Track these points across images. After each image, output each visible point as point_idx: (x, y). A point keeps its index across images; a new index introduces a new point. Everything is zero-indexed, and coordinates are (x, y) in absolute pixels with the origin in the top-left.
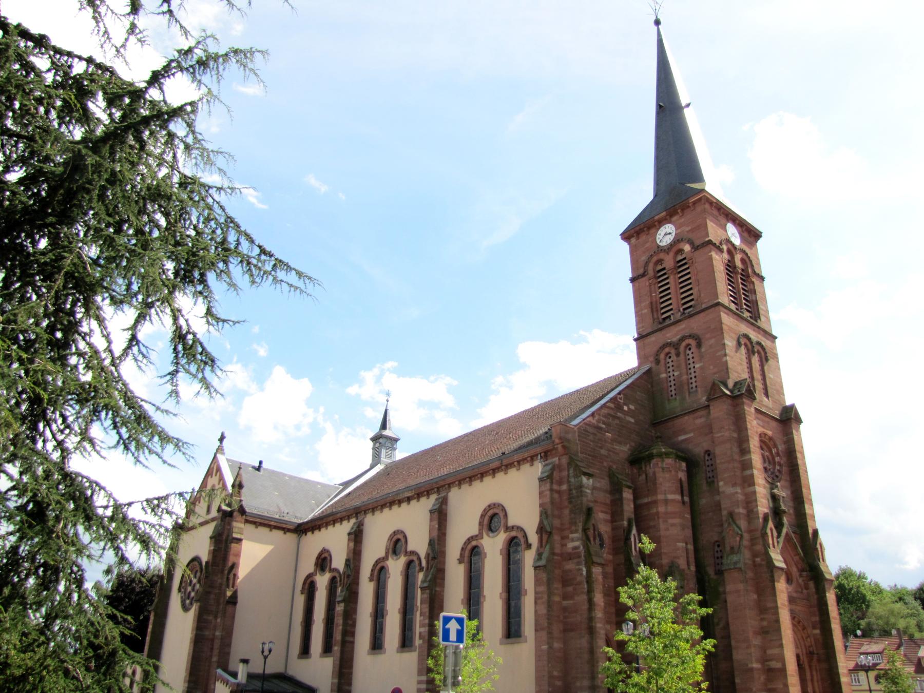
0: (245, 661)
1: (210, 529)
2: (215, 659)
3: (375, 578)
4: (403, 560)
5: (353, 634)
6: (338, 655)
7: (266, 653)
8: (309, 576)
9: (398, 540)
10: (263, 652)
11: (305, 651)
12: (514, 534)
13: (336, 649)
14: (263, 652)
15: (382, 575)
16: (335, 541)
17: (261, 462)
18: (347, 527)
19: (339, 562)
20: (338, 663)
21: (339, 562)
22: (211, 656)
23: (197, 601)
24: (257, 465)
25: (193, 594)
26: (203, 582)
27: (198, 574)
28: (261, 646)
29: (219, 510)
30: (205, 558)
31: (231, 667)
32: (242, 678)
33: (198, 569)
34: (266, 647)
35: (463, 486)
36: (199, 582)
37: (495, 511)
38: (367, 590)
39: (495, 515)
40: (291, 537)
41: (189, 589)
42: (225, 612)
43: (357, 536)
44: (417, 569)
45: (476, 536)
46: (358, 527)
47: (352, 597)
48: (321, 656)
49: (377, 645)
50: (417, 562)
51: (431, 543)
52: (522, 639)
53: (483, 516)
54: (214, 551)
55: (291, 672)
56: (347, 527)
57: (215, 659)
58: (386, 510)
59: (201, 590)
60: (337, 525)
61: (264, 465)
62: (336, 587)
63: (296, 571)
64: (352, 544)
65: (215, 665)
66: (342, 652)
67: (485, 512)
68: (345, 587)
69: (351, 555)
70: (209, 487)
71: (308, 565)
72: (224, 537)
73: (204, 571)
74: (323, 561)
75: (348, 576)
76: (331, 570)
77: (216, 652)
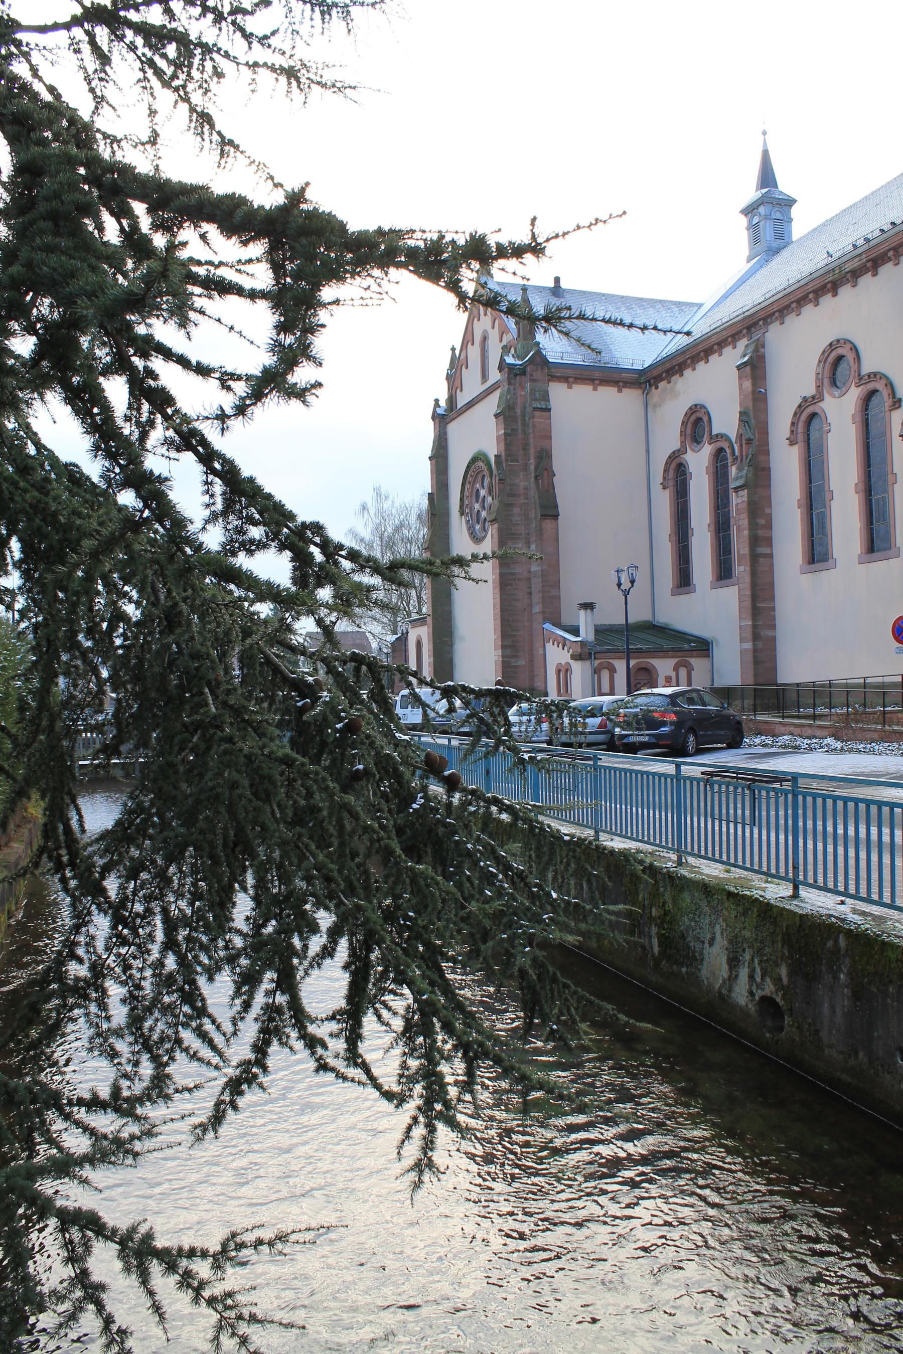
0: (588, 606)
1: (492, 404)
2: (537, 609)
3: (800, 437)
4: (707, 450)
6: (747, 579)
8: (806, 402)
9: (840, 358)
10: (619, 585)
11: (684, 580)
12: (719, 444)
13: (741, 570)
14: (619, 585)
16: (716, 387)
17: (557, 280)
18: (734, 355)
19: (726, 421)
20: (748, 592)
21: (726, 421)
23: (492, 521)
24: (552, 285)
25: (484, 514)
26: (496, 490)
27: (487, 481)
28: (614, 575)
30: (492, 449)
31: (566, 620)
33: (486, 473)
34: (624, 579)
36: (490, 492)
37: (840, 351)
38: (786, 464)
39: (840, 358)
40: (631, 397)
42: (540, 532)
43: (755, 369)
44: (888, 402)
46: (756, 350)
47: (760, 477)
48: (674, 594)
49: (817, 553)
50: (885, 393)
51: (744, 418)
52: (892, 552)
53: (684, 423)
54: (506, 434)
55: (663, 618)
56: (734, 355)
57: (537, 609)
58: (701, 366)
59: (496, 502)
60: (714, 358)
61: (563, 285)
62: (725, 467)
63: (648, 452)
64: (748, 384)
65: (540, 618)
66: (754, 573)
67: (825, 354)
68: (744, 464)
69: (750, 404)
70: (478, 338)
71: (668, 437)
72: (519, 411)
73: (495, 472)
74: (696, 424)
75: (749, 441)
76: (715, 438)
77: (537, 597)
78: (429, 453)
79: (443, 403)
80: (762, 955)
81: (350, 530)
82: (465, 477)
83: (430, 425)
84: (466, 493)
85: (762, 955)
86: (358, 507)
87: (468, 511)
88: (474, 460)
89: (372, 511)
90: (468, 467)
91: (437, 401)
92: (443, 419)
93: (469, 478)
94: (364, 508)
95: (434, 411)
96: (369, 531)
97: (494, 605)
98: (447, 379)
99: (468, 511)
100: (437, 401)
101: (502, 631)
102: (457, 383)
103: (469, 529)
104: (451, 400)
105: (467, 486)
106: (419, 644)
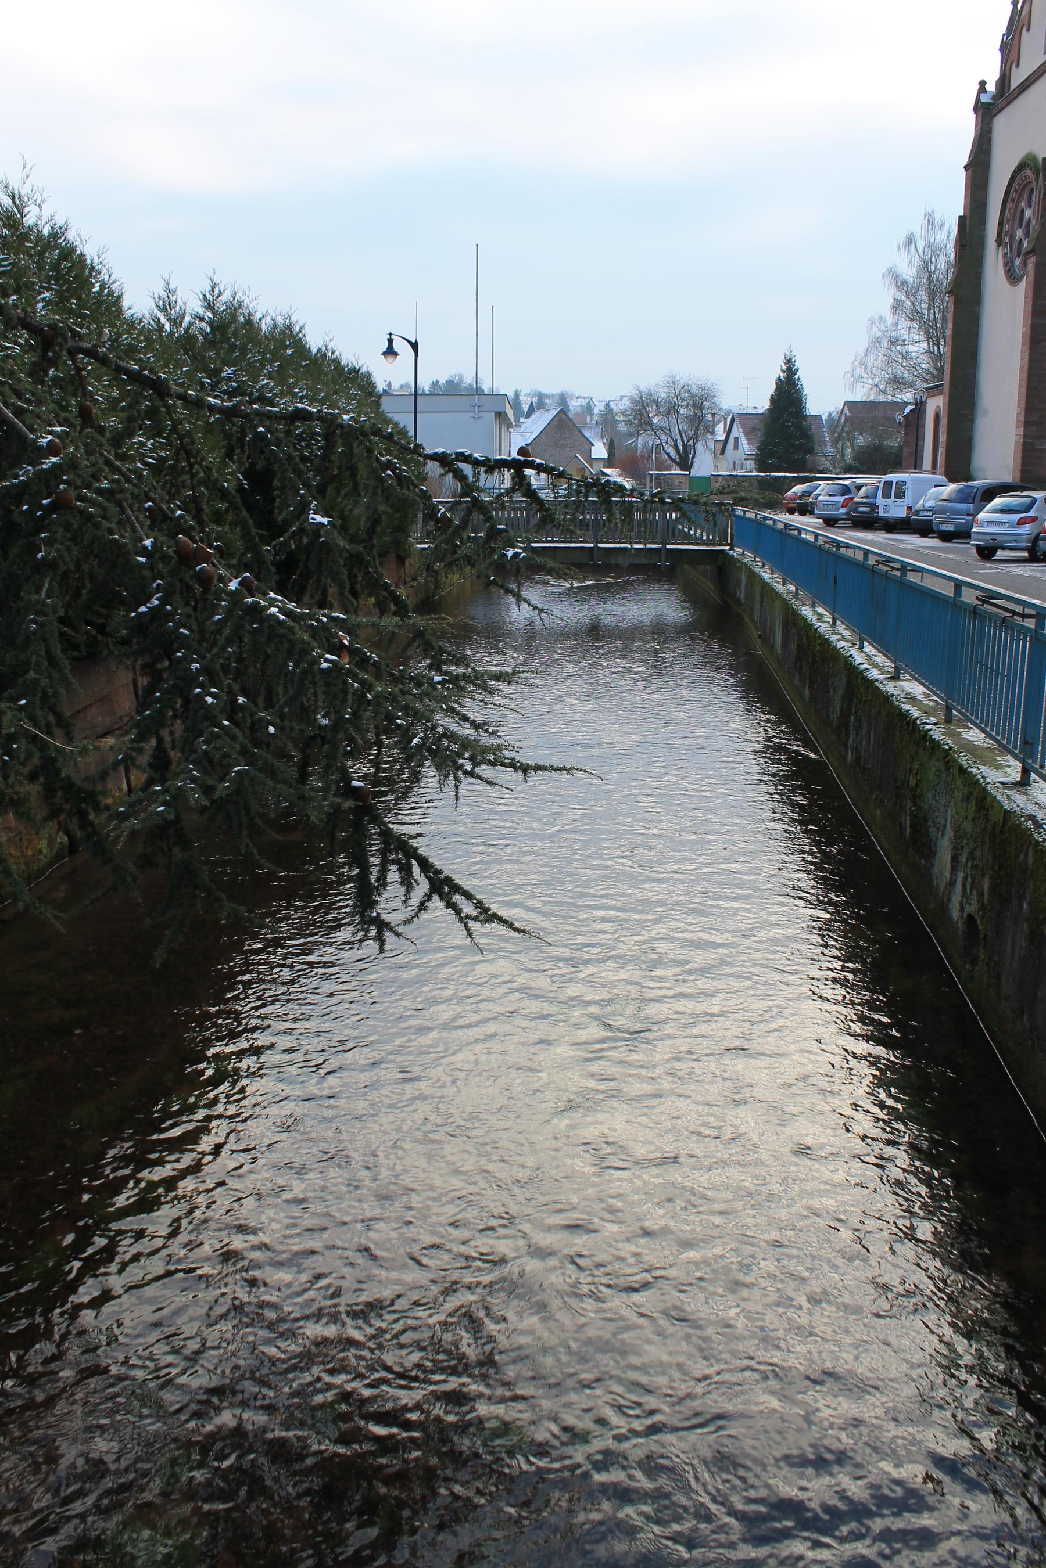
41: (1019, 233)
78: (965, 160)
79: (991, 87)
80: (974, 859)
81: (890, 270)
82: (1007, 193)
83: (972, 117)
84: (1007, 215)
85: (974, 859)
86: (903, 239)
87: (1006, 239)
88: (1021, 167)
89: (921, 244)
90: (1013, 178)
91: (983, 84)
92: (987, 111)
93: (1013, 194)
94: (910, 241)
95: (978, 99)
96: (914, 271)
97: (1021, 367)
98: (1001, 49)
99: (1006, 239)
100: (983, 84)
101: (1027, 404)
102: (1013, 56)
103: (1006, 265)
104: (1004, 80)
105: (1010, 205)
106: (937, 417)
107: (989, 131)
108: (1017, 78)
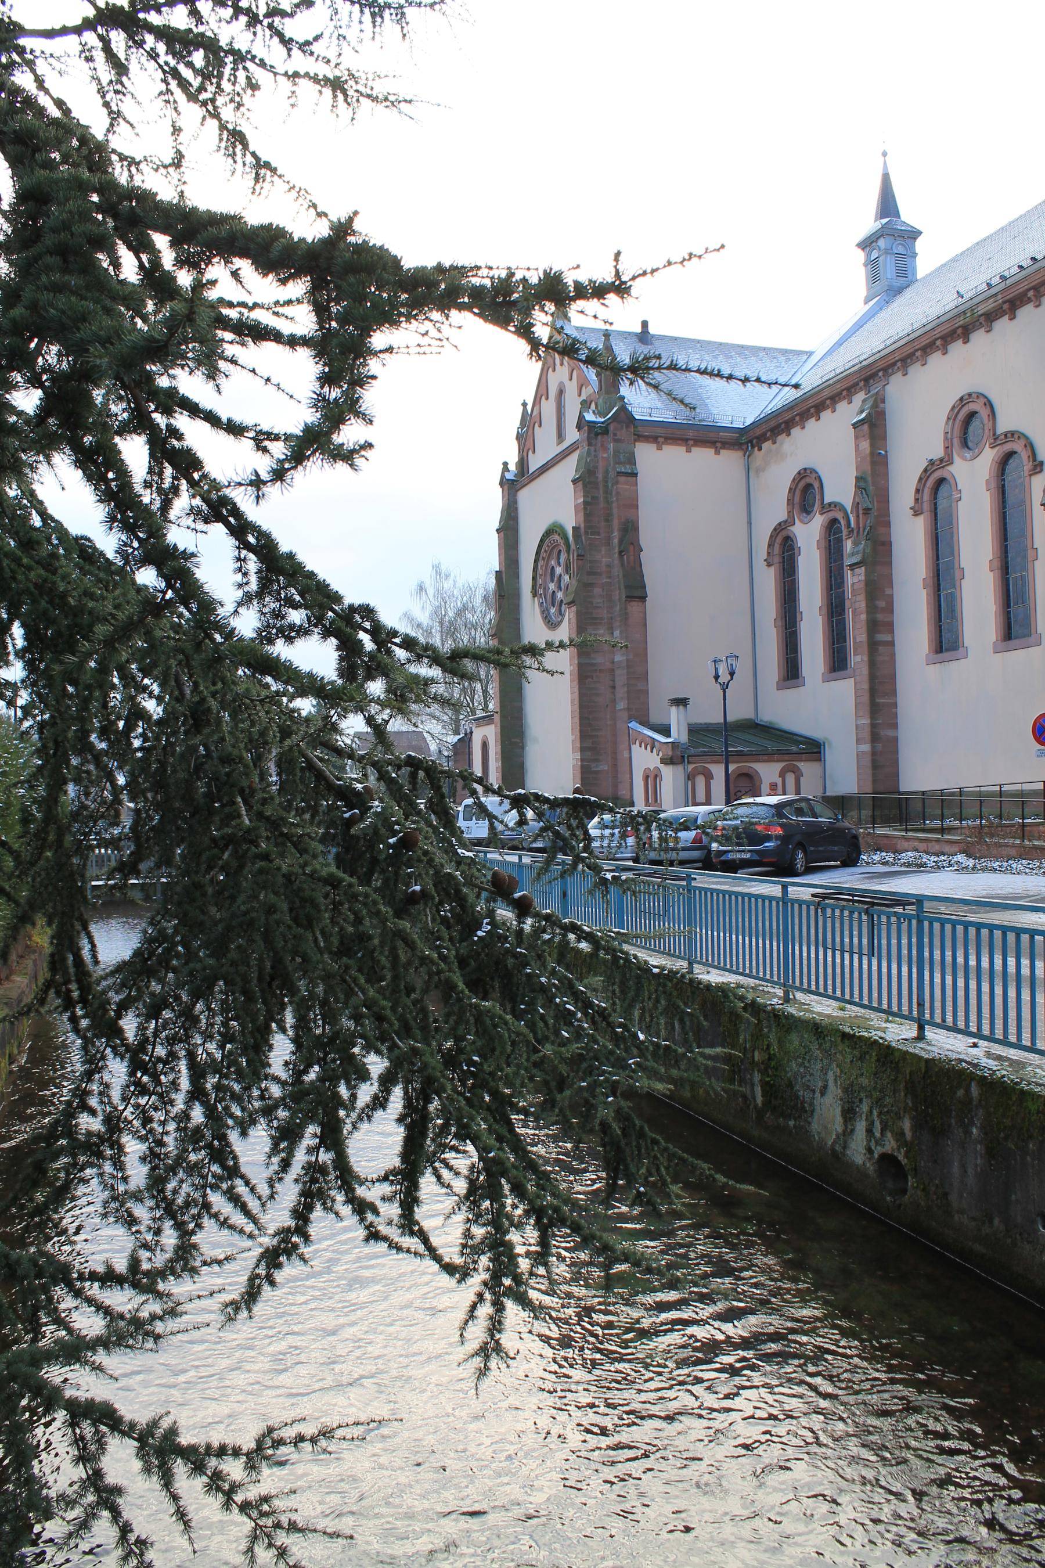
0: (681, 702)
1: (569, 468)
2: (621, 705)
3: (926, 506)
4: (818, 521)
5: (890, 627)
6: (865, 671)
7: (724, 677)
8: (932, 466)
9: (972, 415)
10: (717, 677)
11: (791, 671)
13: (857, 660)
14: (717, 677)
15: (942, 504)
16: (829, 448)
18: (850, 411)
19: (840, 488)
20: (866, 686)
21: (840, 488)
22: (614, 701)
23: (570, 604)
25: (560, 595)
26: (574, 567)
27: (563, 557)
28: (711, 665)
29: (581, 424)
30: (569, 520)
31: (655, 718)
32: (679, 734)
33: (563, 547)
34: (723, 670)
35: (950, 347)
36: (567, 570)
37: (972, 407)
38: (910, 537)
39: (972, 415)
41: (552, 586)
42: (625, 616)
43: (874, 427)
44: (1028, 466)
45: (941, 460)
46: (875, 405)
47: (879, 552)
48: (780, 687)
49: (945, 641)
50: (1024, 455)
51: (861, 483)
52: (1032, 639)
55: (767, 716)
56: (850, 411)
57: (621, 705)
59: (574, 582)
60: (826, 415)
62: (839, 541)
63: (750, 523)
64: (865, 445)
65: (625, 715)
66: (872, 664)
67: (952, 417)
68: (861, 537)
69: (867, 468)
71: (773, 506)
73: (573, 546)
74: (806, 491)
75: (867, 511)
76: (827, 508)
77: (621, 692)
78: (496, 525)
79: (512, 467)
81: (405, 614)
82: (538, 553)
84: (540, 571)
86: (414, 586)
88: (548, 533)
89: (431, 591)
90: (542, 541)
91: (505, 464)
92: (513, 485)
93: (543, 554)
94: (421, 588)
97: (572, 701)
98: (518, 438)
100: (505, 464)
101: (581, 731)
102: (529, 444)
103: (543, 612)
104: (522, 463)
105: (541, 563)
106: (485, 746)
107: (516, 502)
108: (535, 463)
